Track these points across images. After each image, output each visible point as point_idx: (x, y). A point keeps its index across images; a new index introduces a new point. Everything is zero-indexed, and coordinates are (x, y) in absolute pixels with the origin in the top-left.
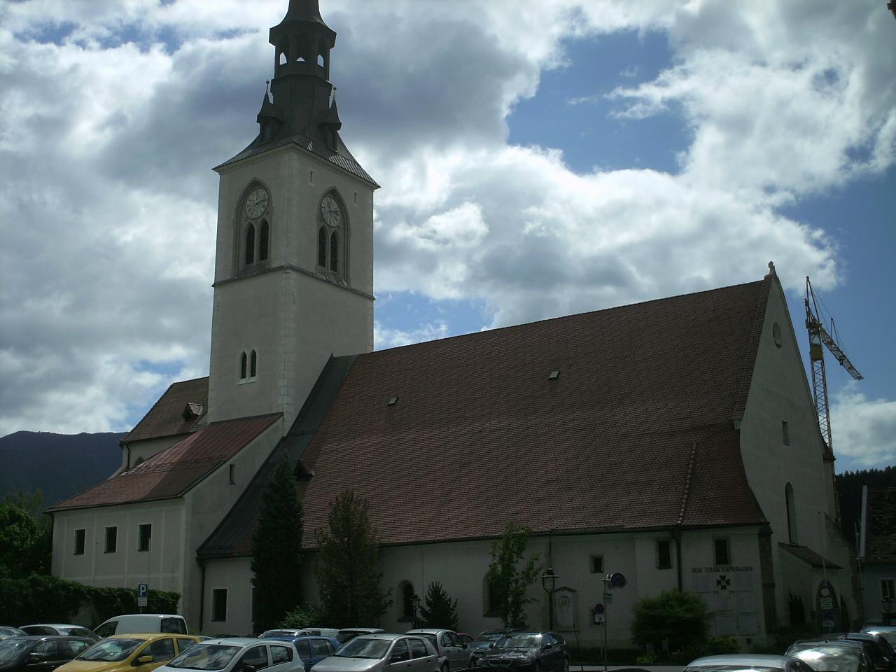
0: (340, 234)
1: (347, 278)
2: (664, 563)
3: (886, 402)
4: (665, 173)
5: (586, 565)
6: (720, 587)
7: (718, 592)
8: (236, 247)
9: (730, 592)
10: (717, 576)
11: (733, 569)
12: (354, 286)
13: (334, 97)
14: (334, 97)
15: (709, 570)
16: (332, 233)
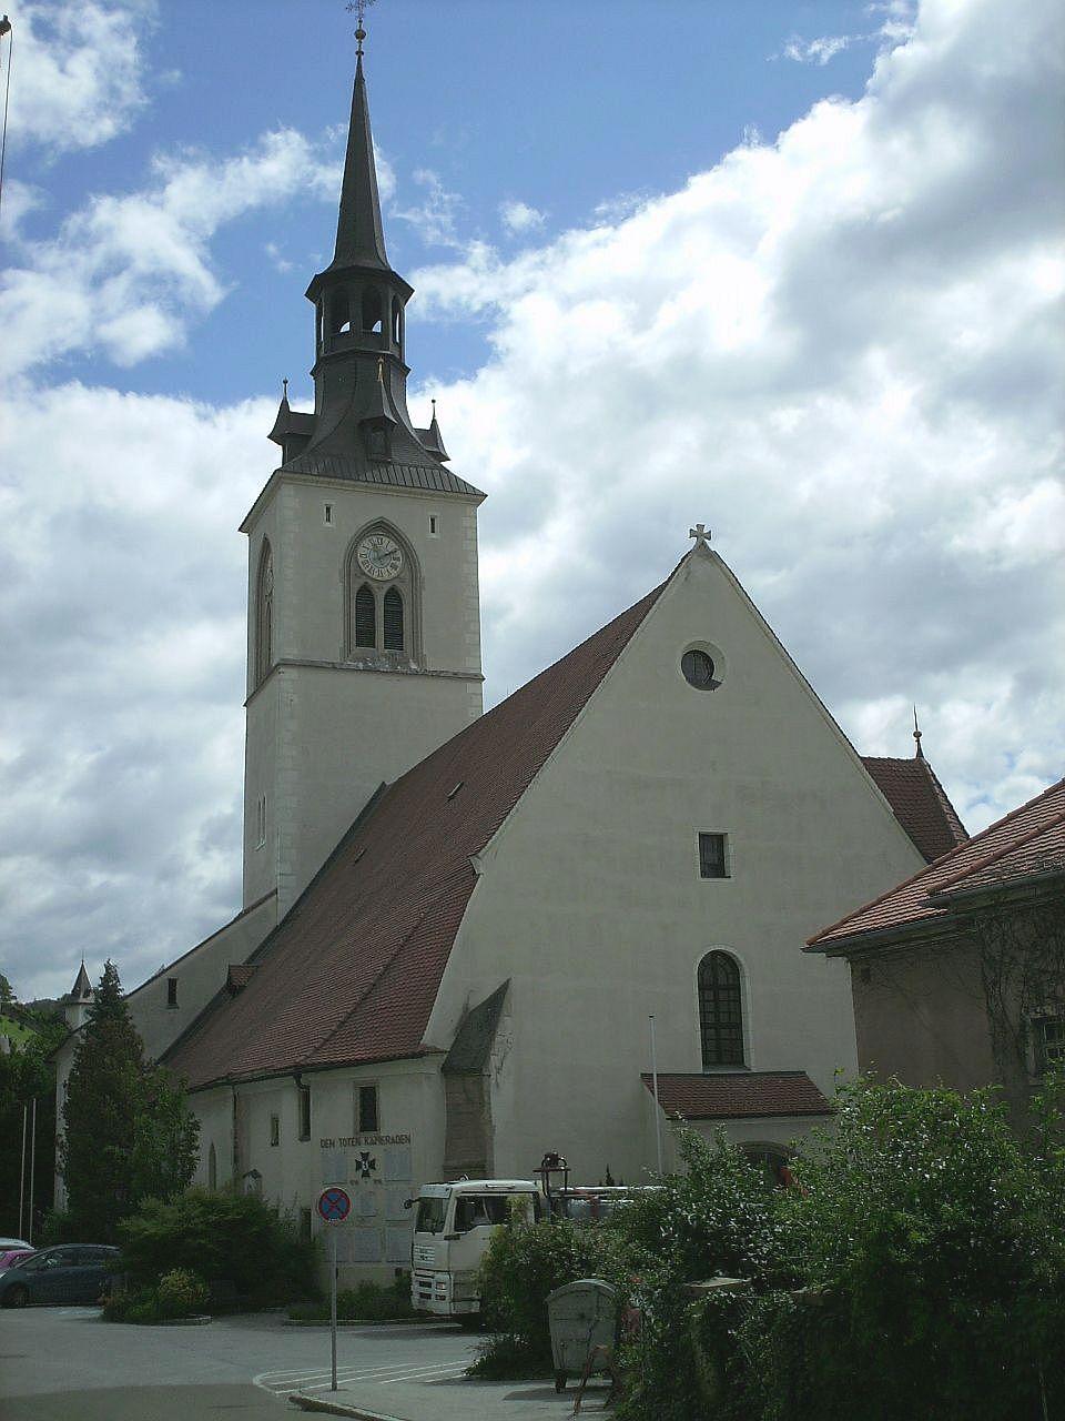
0: (405, 590)
1: (419, 660)
4: (459, 382)
7: (357, 1183)
9: (375, 1181)
10: (354, 1154)
11: (380, 1140)
15: (344, 1142)
16: (384, 592)
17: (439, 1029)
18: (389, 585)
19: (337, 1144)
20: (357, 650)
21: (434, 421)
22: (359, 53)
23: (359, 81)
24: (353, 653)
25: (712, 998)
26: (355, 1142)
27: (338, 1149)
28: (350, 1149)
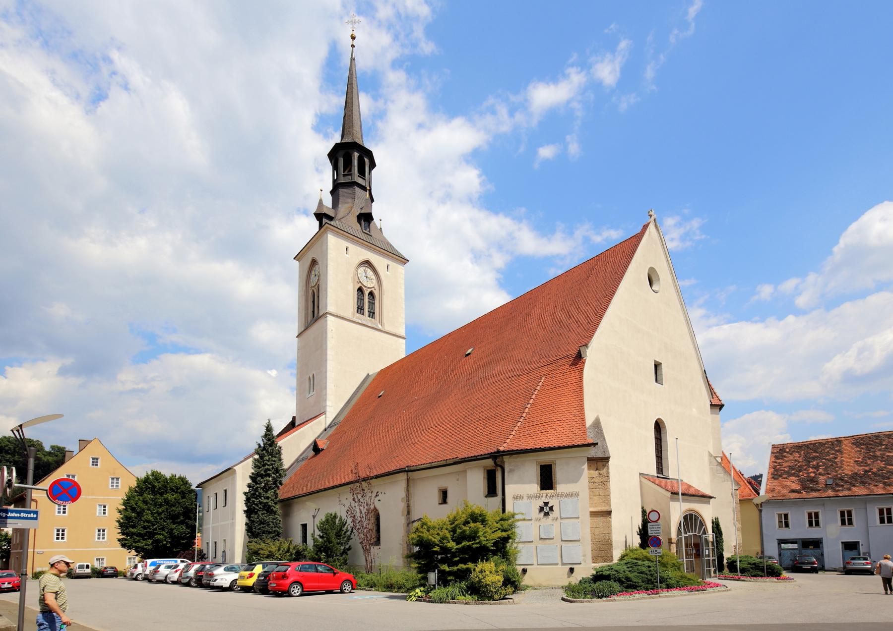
0: (376, 293)
1: (381, 322)
2: (491, 491)
3: (729, 322)
5: (436, 497)
6: (542, 514)
7: (540, 519)
8: (307, 308)
11: (558, 495)
12: (387, 328)
13: (717, 585)
14: (717, 585)
16: (368, 292)
17: (264, 587)
18: (370, 290)
19: (525, 497)
22: (353, 46)
27: (525, 500)
28: (534, 501)
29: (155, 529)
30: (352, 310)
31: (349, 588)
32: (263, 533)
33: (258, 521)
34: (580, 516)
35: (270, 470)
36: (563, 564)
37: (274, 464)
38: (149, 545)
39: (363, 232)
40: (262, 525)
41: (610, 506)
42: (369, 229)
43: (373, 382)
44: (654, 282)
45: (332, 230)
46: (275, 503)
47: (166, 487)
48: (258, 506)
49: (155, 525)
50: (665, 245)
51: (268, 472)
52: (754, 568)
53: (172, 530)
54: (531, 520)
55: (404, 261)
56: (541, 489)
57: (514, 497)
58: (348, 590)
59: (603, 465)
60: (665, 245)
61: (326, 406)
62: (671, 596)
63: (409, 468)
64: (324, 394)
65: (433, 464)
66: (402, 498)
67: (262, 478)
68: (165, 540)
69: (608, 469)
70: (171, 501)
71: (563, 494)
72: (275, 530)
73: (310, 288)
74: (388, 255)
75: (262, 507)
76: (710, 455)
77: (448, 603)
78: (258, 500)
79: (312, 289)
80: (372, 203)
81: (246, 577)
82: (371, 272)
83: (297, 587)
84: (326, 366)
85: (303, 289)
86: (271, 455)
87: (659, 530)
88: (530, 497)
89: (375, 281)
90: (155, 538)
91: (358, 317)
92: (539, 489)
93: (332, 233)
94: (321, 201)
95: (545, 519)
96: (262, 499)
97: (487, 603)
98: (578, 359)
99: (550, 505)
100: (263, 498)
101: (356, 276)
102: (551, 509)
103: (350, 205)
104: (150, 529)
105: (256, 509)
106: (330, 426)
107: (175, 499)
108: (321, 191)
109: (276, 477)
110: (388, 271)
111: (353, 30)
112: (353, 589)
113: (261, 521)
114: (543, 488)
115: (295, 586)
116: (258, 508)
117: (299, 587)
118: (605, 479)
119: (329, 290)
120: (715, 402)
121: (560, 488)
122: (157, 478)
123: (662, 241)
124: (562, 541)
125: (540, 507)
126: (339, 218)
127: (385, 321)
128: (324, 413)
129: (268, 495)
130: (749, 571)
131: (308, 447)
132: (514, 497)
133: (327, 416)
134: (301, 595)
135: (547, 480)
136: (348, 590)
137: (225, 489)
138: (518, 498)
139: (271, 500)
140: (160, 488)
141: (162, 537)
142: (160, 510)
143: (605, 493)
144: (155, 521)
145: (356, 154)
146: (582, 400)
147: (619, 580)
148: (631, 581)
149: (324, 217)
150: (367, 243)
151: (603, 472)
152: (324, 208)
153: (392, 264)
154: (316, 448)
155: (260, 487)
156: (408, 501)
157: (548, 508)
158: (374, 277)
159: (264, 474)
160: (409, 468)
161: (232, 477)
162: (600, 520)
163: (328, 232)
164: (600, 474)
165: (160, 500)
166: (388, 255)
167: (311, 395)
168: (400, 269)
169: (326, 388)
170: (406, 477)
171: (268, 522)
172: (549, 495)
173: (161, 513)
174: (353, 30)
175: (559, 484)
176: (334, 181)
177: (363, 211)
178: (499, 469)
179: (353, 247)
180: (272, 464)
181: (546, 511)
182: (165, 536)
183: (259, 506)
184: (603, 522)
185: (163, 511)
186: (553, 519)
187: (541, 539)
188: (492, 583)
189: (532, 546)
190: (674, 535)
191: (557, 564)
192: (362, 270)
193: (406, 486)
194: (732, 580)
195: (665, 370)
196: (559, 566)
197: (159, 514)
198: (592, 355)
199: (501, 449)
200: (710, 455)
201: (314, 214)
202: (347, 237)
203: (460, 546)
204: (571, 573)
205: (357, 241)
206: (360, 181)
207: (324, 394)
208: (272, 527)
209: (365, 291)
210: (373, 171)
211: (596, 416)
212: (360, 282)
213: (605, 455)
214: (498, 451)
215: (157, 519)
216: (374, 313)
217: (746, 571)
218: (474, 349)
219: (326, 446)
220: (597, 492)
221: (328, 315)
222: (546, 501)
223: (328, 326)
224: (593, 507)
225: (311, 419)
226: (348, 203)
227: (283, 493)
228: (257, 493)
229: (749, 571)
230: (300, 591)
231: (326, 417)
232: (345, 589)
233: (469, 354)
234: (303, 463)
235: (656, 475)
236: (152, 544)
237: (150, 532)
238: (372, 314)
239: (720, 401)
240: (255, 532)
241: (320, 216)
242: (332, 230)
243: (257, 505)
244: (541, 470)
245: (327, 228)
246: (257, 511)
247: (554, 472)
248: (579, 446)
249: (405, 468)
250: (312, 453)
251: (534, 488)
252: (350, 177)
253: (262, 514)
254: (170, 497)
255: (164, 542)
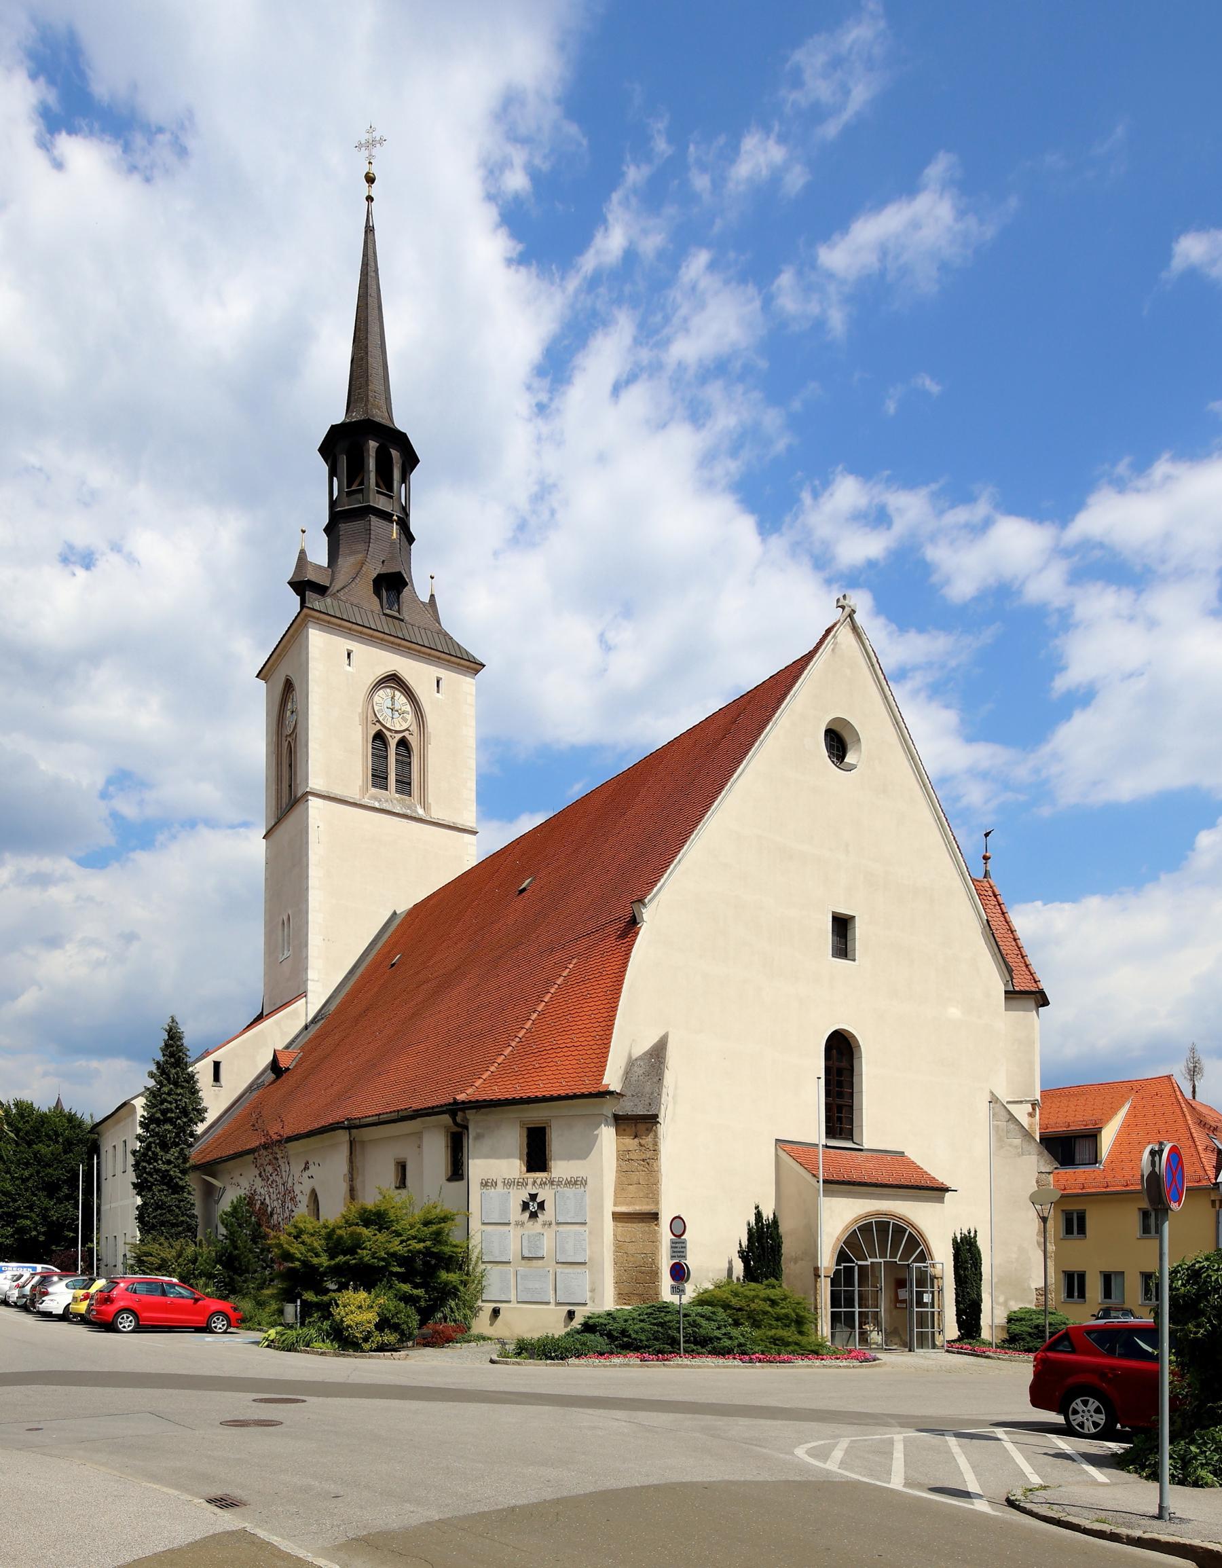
0: (413, 741)
1: (424, 804)
6: (527, 1214)
7: (523, 1224)
11: (552, 1183)
12: (436, 814)
16: (396, 740)
18: (401, 735)
19: (500, 1184)
20: (374, 791)
21: (432, 596)
22: (370, 199)
23: (369, 230)
24: (369, 792)
25: (1017, 989)
26: (522, 1184)
29: (18, 1208)
30: (361, 783)
31: (223, 1325)
32: (161, 1226)
33: (152, 1204)
34: (587, 1221)
35: (171, 1111)
36: (558, 1304)
37: (180, 1100)
38: (7, 1238)
39: (384, 614)
40: (159, 1212)
41: (657, 1203)
42: (399, 605)
43: (401, 924)
44: (849, 747)
45: (318, 619)
46: (184, 1172)
47: (37, 1131)
48: (152, 1177)
49: (17, 1201)
50: (877, 666)
51: (169, 1115)
52: (1035, 1334)
53: (47, 1209)
54: (509, 1224)
55: (472, 666)
56: (528, 1171)
57: (482, 1183)
58: (220, 1328)
59: (647, 1130)
60: (877, 666)
61: (308, 980)
62: (687, 1366)
63: (352, 1122)
64: (304, 956)
65: (381, 1117)
66: (345, 1175)
67: (158, 1126)
68: (35, 1229)
69: (656, 1136)
70: (45, 1156)
71: (561, 1180)
72: (183, 1221)
73: (284, 738)
74: (439, 658)
75: (158, 1178)
76: (994, 1100)
77: (299, 1352)
78: (151, 1166)
79: (289, 739)
80: (411, 544)
81: (79, 1300)
82: (402, 696)
83: (128, 1318)
84: (307, 900)
85: (272, 740)
86: (176, 1084)
87: (683, 1252)
88: (508, 1183)
89: (410, 717)
90: (19, 1224)
91: (374, 796)
92: (524, 1169)
93: (318, 626)
94: (302, 554)
95: (531, 1223)
96: (159, 1164)
97: (350, 1356)
98: (632, 925)
99: (539, 1200)
100: (160, 1162)
101: (370, 711)
102: (541, 1206)
103: (360, 557)
104: (9, 1207)
105: (150, 1182)
106: (314, 1021)
107: (52, 1154)
108: (304, 532)
109: (182, 1125)
110: (438, 692)
111: (370, 163)
112: (229, 1325)
113: (157, 1204)
114: (530, 1169)
115: (125, 1316)
116: (152, 1180)
117: (131, 1318)
118: (649, 1154)
119: (311, 744)
120: (1022, 984)
121: (560, 1168)
122: (22, 1113)
123: (870, 658)
124: (557, 1263)
125: (523, 1201)
126: (335, 591)
127: (431, 799)
128: (304, 994)
129: (168, 1157)
130: (1023, 1339)
131: (267, 1066)
132: (482, 1183)
133: (309, 1000)
134: (132, 1331)
135: (537, 1159)
136: (220, 1328)
137: (124, 1139)
138: (579, 1183)
139: (175, 1167)
140: (27, 1133)
141: (28, 1222)
142: (26, 1173)
143: (649, 1179)
144: (19, 1194)
145: (373, 445)
146: (614, 1009)
147: (610, 1335)
148: (629, 1336)
149: (307, 588)
150: (392, 639)
151: (648, 1140)
152: (310, 568)
153: (446, 675)
154: (275, 1066)
155: (154, 1143)
156: (352, 1180)
157: (536, 1205)
158: (408, 708)
159: (162, 1118)
160: (352, 1122)
161: (131, 1119)
162: (637, 1228)
163: (310, 624)
164: (641, 1145)
165: (28, 1155)
166: (439, 658)
167: (285, 956)
168: (466, 684)
169: (306, 945)
170: (347, 1138)
171: (170, 1206)
172: (538, 1181)
173: (28, 1179)
174: (370, 163)
175: (555, 1160)
176: (333, 504)
177: (384, 570)
178: (466, 1131)
179: (361, 650)
180: (176, 1101)
181: (533, 1210)
182: (34, 1222)
183: (155, 1177)
184: (642, 1233)
185: (31, 1175)
186: (544, 1225)
187: (523, 1258)
188: (357, 1324)
189: (510, 1269)
190: (827, 1260)
191: (548, 1303)
192: (383, 696)
193: (349, 1154)
194: (972, 1355)
195: (861, 933)
196: (552, 1306)
197: (25, 1180)
198: (653, 916)
199: (461, 1097)
200: (994, 1100)
201: (289, 583)
202: (350, 629)
203: (333, 1263)
204: (568, 1321)
205: (371, 636)
206: (381, 503)
207: (304, 956)
208: (177, 1215)
209: (390, 739)
210: (415, 476)
211: (662, 1034)
212: (379, 721)
213: (648, 1111)
214: (455, 1102)
215: (21, 1189)
216: (410, 784)
217: (1017, 1341)
218: (534, 879)
219: (294, 1063)
220: (634, 1177)
221: (310, 798)
222: (533, 1192)
223: (311, 820)
224: (627, 1204)
225: (286, 1003)
226: (359, 552)
227: (195, 1154)
228: (150, 1153)
229: (1023, 1339)
230: (133, 1324)
231: (307, 1003)
232: (216, 1327)
233: (524, 889)
234: (255, 1094)
235: (823, 1141)
236: (12, 1236)
237: (9, 1213)
238: (404, 785)
239: (1036, 982)
240: (149, 1222)
241: (301, 586)
242: (318, 619)
243: (150, 1174)
244: (529, 1136)
245: (307, 616)
246: (151, 1186)
247: (447, 1153)
248: (583, 1096)
249: (343, 1122)
250: (273, 1076)
251: (514, 1167)
252: (360, 496)
253: (160, 1191)
254: (44, 1149)
255: (34, 1233)
